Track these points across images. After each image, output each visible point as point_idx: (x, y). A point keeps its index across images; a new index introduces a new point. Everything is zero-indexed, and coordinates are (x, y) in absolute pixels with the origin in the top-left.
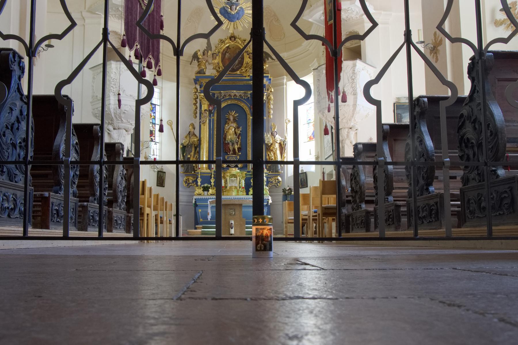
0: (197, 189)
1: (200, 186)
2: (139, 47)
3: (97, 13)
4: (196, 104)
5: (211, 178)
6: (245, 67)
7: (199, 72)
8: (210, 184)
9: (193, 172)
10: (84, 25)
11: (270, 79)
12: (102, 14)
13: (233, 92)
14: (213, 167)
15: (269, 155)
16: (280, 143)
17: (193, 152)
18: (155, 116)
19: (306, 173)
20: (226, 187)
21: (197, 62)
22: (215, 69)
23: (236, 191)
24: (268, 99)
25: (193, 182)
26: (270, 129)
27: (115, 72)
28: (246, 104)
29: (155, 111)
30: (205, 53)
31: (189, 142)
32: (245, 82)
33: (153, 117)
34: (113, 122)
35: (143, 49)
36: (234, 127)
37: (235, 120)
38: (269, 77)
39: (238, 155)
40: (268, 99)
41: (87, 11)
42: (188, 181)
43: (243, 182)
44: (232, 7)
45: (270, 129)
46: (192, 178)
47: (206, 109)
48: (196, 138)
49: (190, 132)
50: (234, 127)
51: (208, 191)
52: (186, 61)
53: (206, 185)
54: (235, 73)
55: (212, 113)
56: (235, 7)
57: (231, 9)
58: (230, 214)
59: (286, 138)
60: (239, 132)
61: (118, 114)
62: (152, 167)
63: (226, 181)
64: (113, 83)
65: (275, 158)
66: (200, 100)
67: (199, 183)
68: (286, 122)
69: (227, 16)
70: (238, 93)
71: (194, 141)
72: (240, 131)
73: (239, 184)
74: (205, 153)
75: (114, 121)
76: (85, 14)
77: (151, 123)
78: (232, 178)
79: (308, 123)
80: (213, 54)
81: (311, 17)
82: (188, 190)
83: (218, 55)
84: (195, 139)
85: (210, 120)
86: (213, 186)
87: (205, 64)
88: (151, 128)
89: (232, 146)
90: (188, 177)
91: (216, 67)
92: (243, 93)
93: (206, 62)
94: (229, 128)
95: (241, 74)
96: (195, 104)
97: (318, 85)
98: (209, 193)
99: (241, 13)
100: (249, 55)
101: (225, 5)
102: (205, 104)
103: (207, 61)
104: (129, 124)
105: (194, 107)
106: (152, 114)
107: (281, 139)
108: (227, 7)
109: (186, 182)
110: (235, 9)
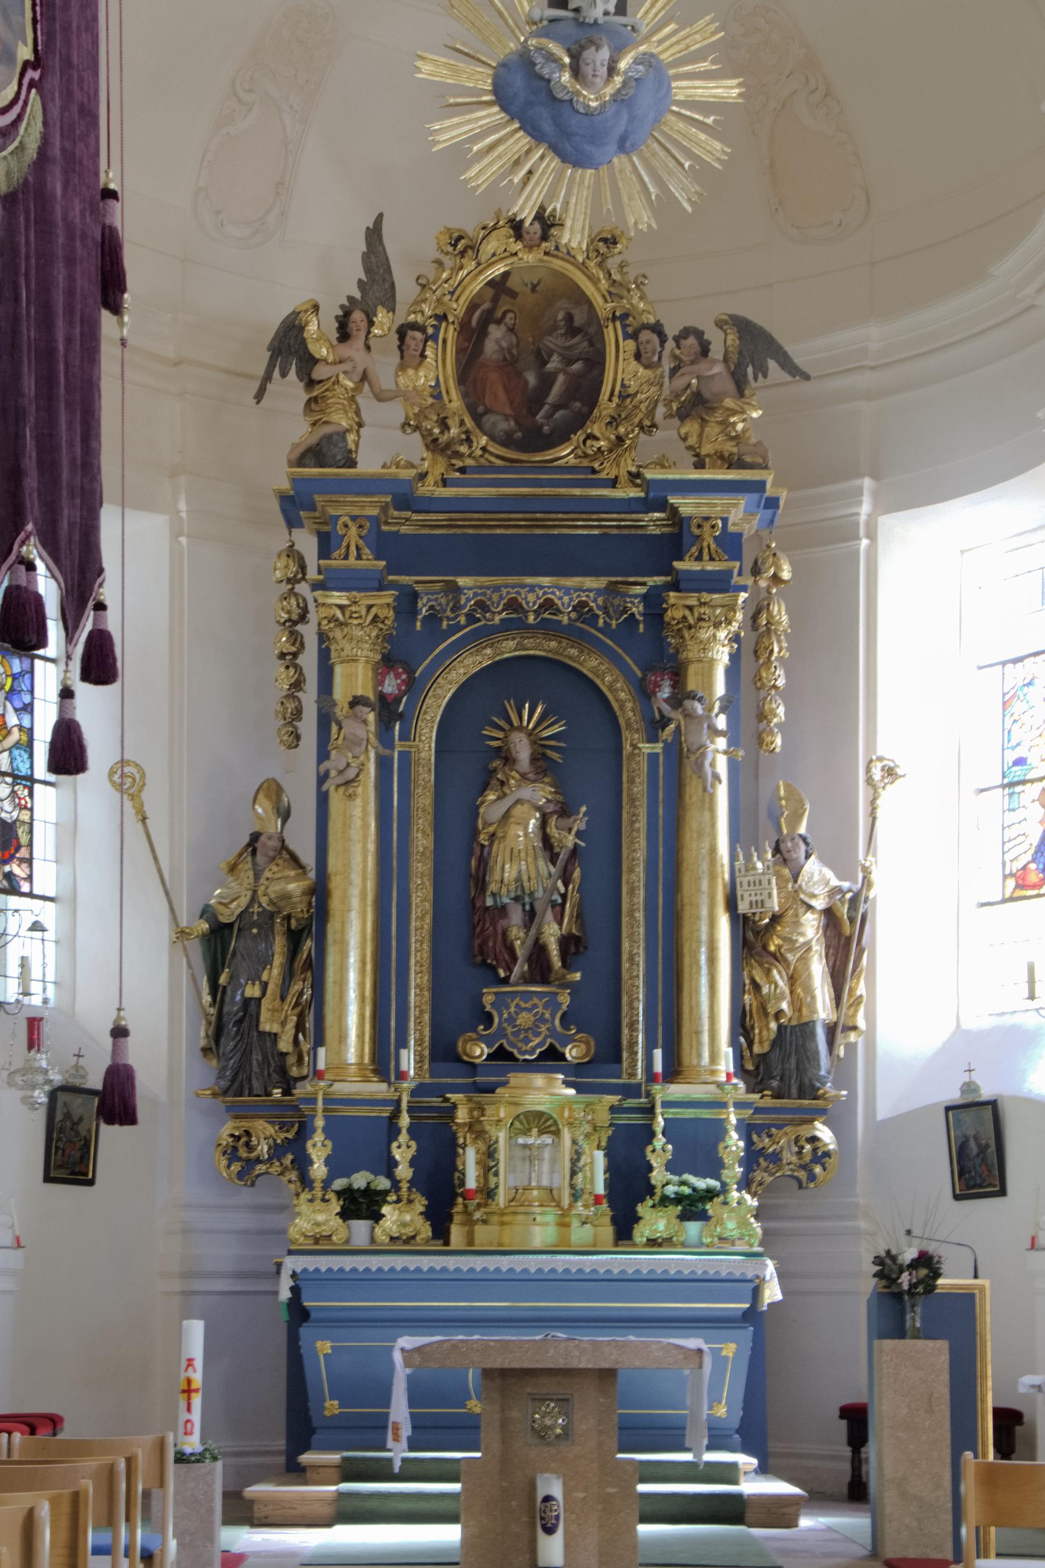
1: (327, 1184)
4: (295, 655)
5: (393, 1132)
6: (614, 421)
9: (277, 1093)
13: (532, 588)
15: (756, 987)
16: (829, 913)
18: (30, 731)
19: (993, 1104)
20: (490, 1194)
22: (417, 428)
23: (550, 1218)
25: (277, 1151)
29: (27, 699)
31: (254, 899)
32: (611, 520)
33: (15, 735)
36: (539, 809)
42: (247, 1144)
44: (589, 54)
46: (271, 1130)
47: (360, 692)
48: (296, 879)
49: (255, 837)
50: (539, 809)
51: (377, 1217)
53: (360, 1180)
54: (549, 455)
55: (401, 716)
56: (605, 54)
57: (576, 72)
58: (541, 1434)
59: (867, 883)
60: (570, 840)
62: (19, 1079)
63: (490, 1153)
65: (797, 1005)
66: (323, 637)
67: (319, 1170)
68: (869, 781)
69: (547, 126)
70: (567, 591)
71: (286, 897)
72: (579, 835)
73: (573, 1173)
74: (355, 903)
78: (526, 1132)
80: (402, 332)
82: (246, 1195)
83: (434, 337)
84: (292, 886)
85: (384, 765)
86: (404, 1186)
88: (7, 806)
90: (245, 1124)
91: (422, 415)
92: (599, 592)
93: (357, 389)
94: (507, 815)
95: (585, 463)
96: (290, 658)
98: (378, 1231)
100: (634, 336)
101: (533, 42)
102: (354, 660)
103: (364, 377)
105: (284, 678)
107: (835, 882)
108: (551, 58)
109: (232, 1154)
110: (603, 71)
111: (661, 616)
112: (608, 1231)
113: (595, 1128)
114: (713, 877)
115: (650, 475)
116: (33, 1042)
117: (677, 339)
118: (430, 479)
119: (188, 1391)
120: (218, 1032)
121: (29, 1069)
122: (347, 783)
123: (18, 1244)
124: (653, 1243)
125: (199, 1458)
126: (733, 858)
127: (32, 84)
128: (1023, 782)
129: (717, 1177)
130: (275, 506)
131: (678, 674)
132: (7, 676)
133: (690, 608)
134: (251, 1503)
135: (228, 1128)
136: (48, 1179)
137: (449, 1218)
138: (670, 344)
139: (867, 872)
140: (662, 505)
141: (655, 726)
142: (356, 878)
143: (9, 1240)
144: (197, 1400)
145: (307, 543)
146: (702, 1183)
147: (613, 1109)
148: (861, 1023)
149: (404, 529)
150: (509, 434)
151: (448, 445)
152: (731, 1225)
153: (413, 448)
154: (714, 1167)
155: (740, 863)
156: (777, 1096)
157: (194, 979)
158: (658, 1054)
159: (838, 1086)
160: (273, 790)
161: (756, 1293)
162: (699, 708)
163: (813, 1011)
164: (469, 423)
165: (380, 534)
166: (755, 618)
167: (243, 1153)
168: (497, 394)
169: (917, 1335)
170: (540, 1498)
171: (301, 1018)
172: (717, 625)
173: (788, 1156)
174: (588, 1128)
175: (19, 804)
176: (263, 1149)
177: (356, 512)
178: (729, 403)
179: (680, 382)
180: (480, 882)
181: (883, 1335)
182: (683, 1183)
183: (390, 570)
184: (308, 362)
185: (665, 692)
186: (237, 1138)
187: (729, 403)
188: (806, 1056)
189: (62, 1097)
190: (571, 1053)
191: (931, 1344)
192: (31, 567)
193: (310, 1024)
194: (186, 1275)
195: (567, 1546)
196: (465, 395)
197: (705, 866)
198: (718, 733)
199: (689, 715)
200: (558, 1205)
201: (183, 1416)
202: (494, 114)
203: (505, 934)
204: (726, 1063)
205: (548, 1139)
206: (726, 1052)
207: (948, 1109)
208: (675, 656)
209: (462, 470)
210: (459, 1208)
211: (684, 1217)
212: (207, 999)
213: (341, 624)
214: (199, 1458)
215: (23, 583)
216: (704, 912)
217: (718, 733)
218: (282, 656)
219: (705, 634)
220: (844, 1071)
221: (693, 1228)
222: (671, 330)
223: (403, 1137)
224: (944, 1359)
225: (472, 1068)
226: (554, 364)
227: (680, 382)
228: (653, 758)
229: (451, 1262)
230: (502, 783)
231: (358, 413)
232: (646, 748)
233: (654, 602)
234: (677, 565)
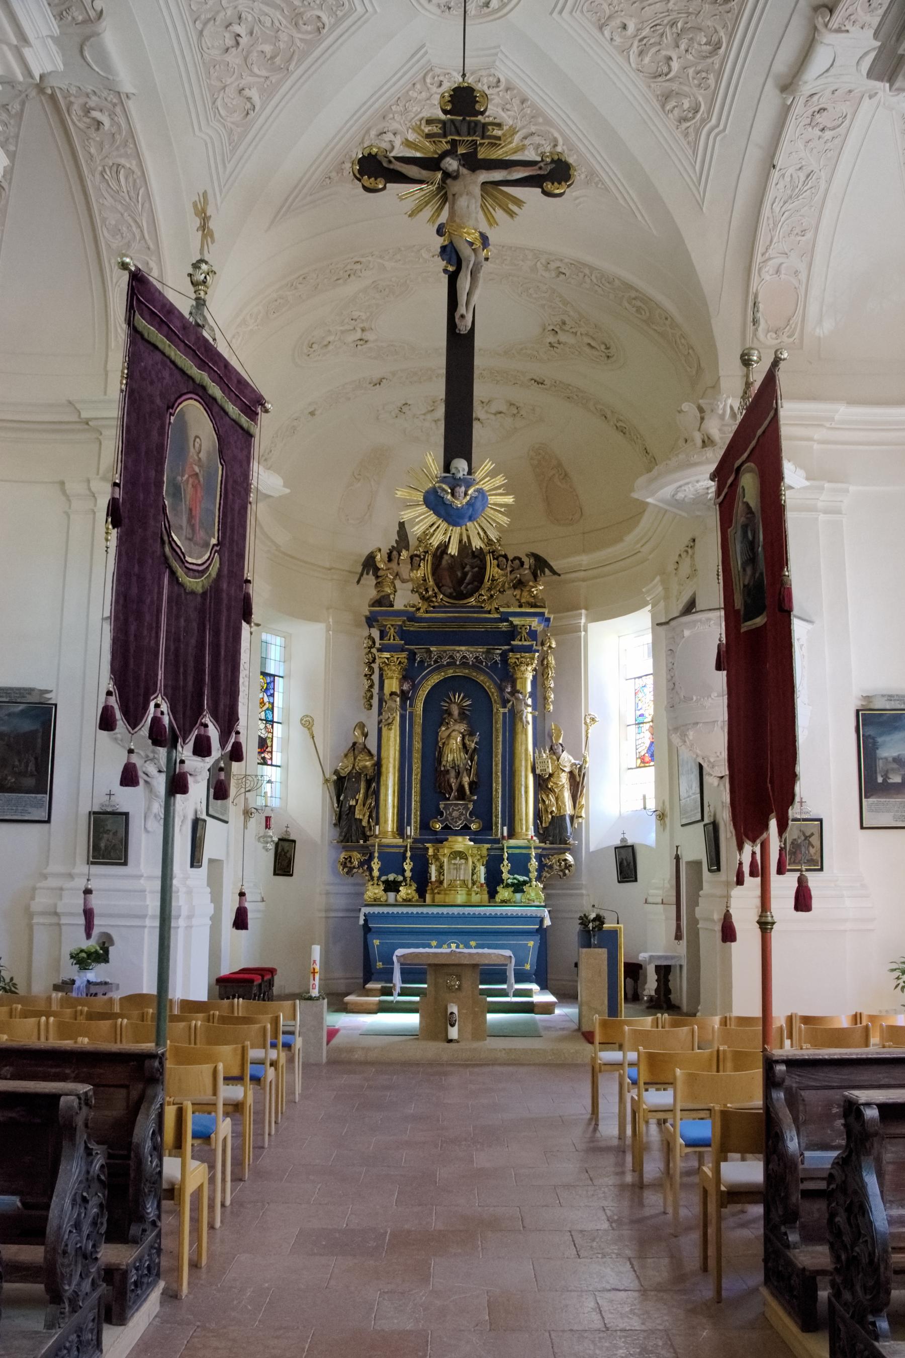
0: (370, 887)
1: (379, 878)
2: (164, 707)
4: (371, 675)
5: (405, 859)
6: (490, 589)
7: (378, 602)
8: (404, 876)
9: (361, 842)
11: (548, 620)
13: (458, 651)
14: (409, 833)
15: (544, 801)
16: (571, 773)
17: (362, 791)
18: (273, 704)
19: (632, 847)
20: (441, 882)
21: (373, 578)
22: (417, 591)
23: (464, 892)
24: (542, 664)
25: (361, 864)
26: (547, 738)
28: (491, 678)
29: (272, 691)
30: (393, 557)
31: (353, 767)
32: (489, 626)
33: (267, 705)
35: (180, 708)
36: (462, 733)
37: (463, 716)
38: (546, 615)
39: (470, 801)
40: (542, 664)
42: (350, 861)
43: (482, 870)
44: (457, 489)
45: (547, 738)
46: (359, 856)
47: (394, 690)
48: (369, 760)
49: (354, 744)
50: (462, 733)
51: (398, 891)
52: (350, 572)
53: (391, 877)
54: (465, 602)
55: (409, 698)
56: (463, 489)
57: (453, 494)
58: (450, 988)
59: (585, 761)
60: (473, 745)
62: (262, 840)
63: (441, 867)
65: (559, 809)
66: (381, 669)
67: (376, 873)
68: (586, 723)
69: (443, 512)
70: (471, 652)
71: (365, 767)
72: (476, 743)
73: (473, 875)
74: (391, 769)
77: (261, 719)
78: (455, 858)
79: (639, 724)
80: (412, 558)
81: (652, 494)
82: (351, 880)
83: (424, 559)
84: (367, 763)
85: (403, 717)
86: (408, 879)
87: (393, 583)
88: (263, 731)
89: (457, 778)
90: (349, 854)
91: (419, 586)
92: (483, 652)
93: (395, 578)
94: (449, 736)
95: (479, 604)
96: (369, 676)
97: (670, 665)
98: (398, 897)
99: (478, 504)
100: (497, 559)
101: (437, 485)
102: (392, 678)
103: (397, 574)
105: (367, 684)
106: (266, 699)
107: (573, 761)
108: (443, 490)
109: (344, 865)
110: (463, 495)
111: (507, 660)
112: (486, 897)
113: (482, 857)
114: (526, 760)
115: (502, 610)
116: (268, 826)
117: (512, 561)
118: (422, 611)
119: (314, 973)
120: (340, 818)
121: (265, 836)
122: (389, 724)
124: (503, 901)
125: (317, 999)
126: (534, 753)
127: (216, 551)
128: (643, 723)
129: (528, 876)
130: (364, 619)
131: (514, 683)
133: (518, 659)
134: (347, 1004)
135: (343, 855)
136: (275, 874)
137: (426, 891)
138: (510, 562)
139: (585, 758)
140: (507, 621)
141: (505, 703)
142: (391, 760)
143: (259, 899)
144: (317, 976)
145: (376, 634)
146: (521, 878)
147: (488, 849)
148: (583, 815)
149: (412, 629)
150: (451, 594)
151: (429, 598)
152: (533, 894)
153: (416, 599)
154: (526, 872)
155: (537, 755)
156: (551, 843)
157: (331, 798)
158: (505, 828)
159: (574, 839)
160: (361, 726)
161: (542, 920)
162: (521, 696)
163: (565, 811)
164: (436, 590)
165: (403, 630)
166: (542, 661)
167: (348, 865)
168: (447, 581)
169: (596, 946)
170: (449, 1012)
171: (371, 812)
172: (527, 665)
173: (556, 867)
174: (479, 857)
176: (356, 863)
177: (393, 623)
178: (531, 583)
179: (513, 576)
180: (440, 762)
181: (584, 946)
182: (515, 879)
183: (406, 644)
184: (376, 569)
185: (509, 690)
186: (346, 859)
187: (531, 583)
188: (563, 828)
189: (281, 843)
190: (473, 827)
191: (600, 950)
192: (206, 726)
193: (374, 815)
194: (327, 911)
195: (459, 1030)
196: (435, 580)
197: (523, 756)
198: (529, 706)
199: (517, 699)
200: (467, 887)
201: (312, 982)
202: (424, 508)
203: (448, 780)
204: (531, 832)
205: (463, 861)
206: (531, 827)
207: (616, 848)
208: (512, 676)
209: (434, 607)
210: (429, 888)
211: (514, 892)
212: (336, 805)
213: (387, 665)
214: (317, 999)
215: (202, 733)
216: (523, 774)
217: (529, 706)
218: (366, 675)
219: (523, 668)
220: (577, 833)
221: (518, 896)
222: (510, 557)
223: (408, 861)
224: (606, 956)
225: (435, 832)
226: (467, 568)
227: (513, 576)
228: (504, 714)
229: (425, 910)
230: (447, 724)
231: (395, 587)
232: (502, 710)
233: (504, 655)
234: (513, 642)
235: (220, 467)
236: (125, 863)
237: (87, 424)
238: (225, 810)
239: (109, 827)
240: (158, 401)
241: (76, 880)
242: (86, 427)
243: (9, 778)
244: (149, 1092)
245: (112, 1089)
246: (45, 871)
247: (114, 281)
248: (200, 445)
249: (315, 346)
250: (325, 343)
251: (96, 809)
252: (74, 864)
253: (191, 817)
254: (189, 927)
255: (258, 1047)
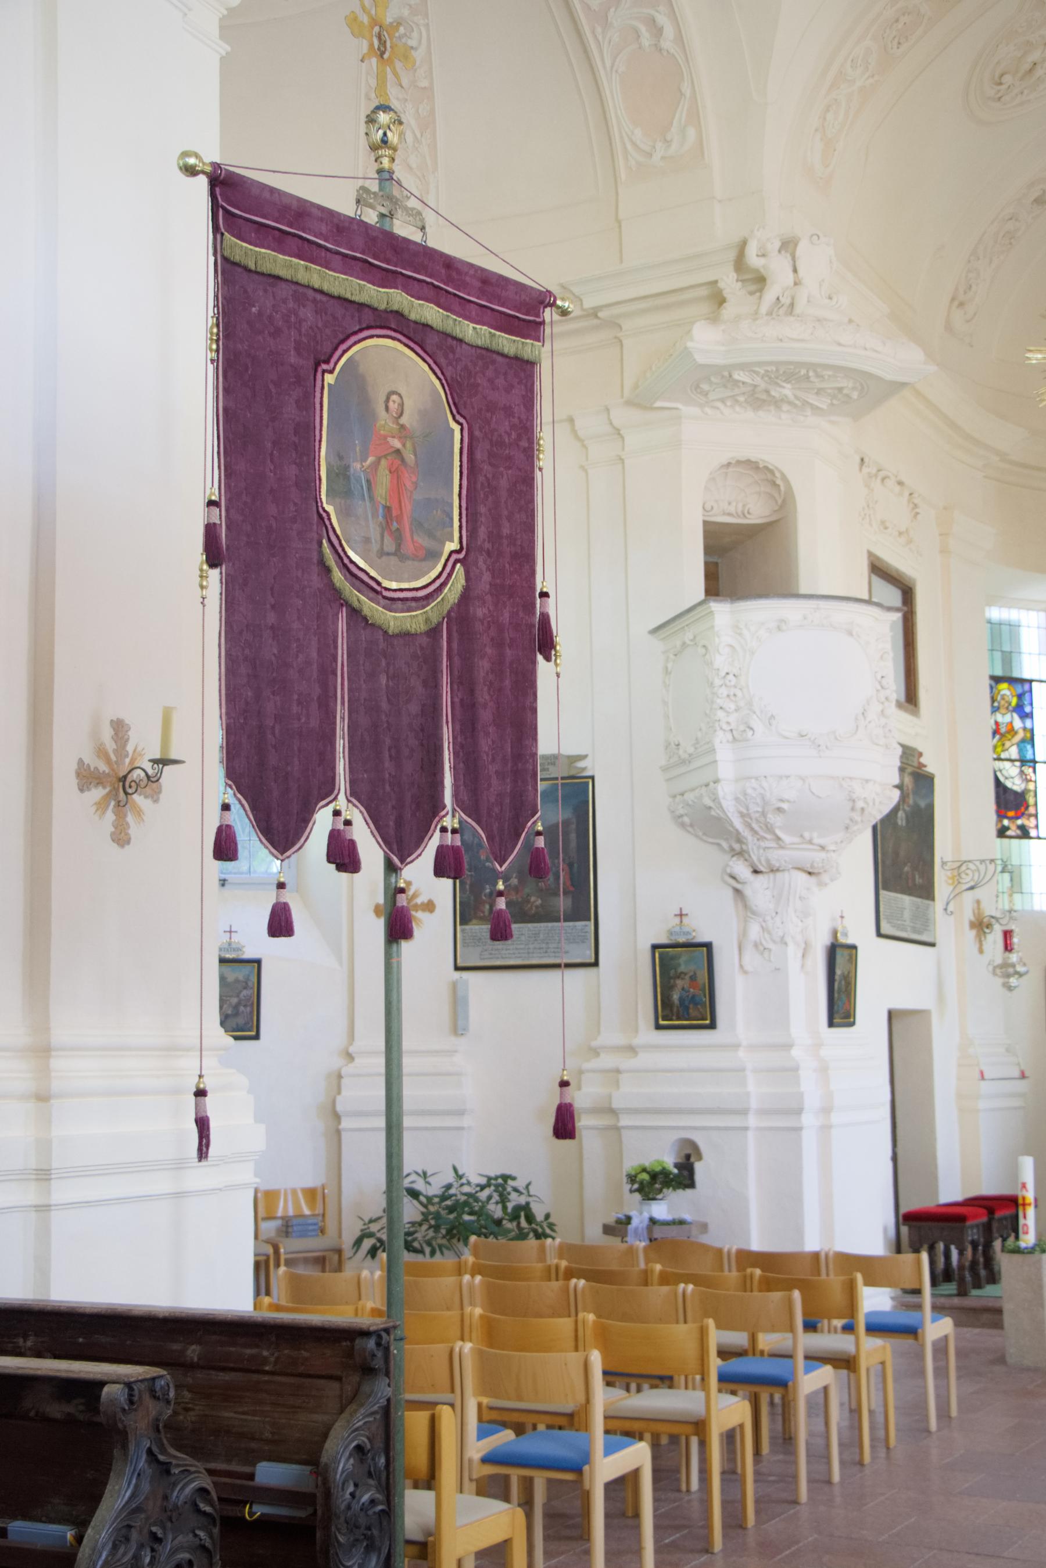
3: (658, 404)
10: (622, 460)
12: (679, 406)
18: (1032, 731)
27: (731, 646)
33: (1021, 735)
34: (744, 847)
41: (629, 403)
61: (754, 816)
62: (998, 971)
64: (724, 691)
75: (746, 844)
76: (621, 416)
88: (1018, 781)
104: (811, 847)
121: (1005, 965)
123: (1023, 1076)
132: (1013, 696)
143: (1017, 1073)
175: (1026, 779)
235: (457, 428)
236: (712, 1026)
237: (596, 317)
238: (924, 921)
239: (682, 968)
240: (293, 359)
241: (602, 1055)
242: (596, 321)
243: (533, 899)
244: (366, 1388)
245: (322, 1382)
246: (594, 1044)
247: (608, 64)
248: (402, 405)
249: (1007, 79)
250: (1027, 66)
251: (663, 940)
252: (636, 1030)
253: (821, 942)
254: (826, 1129)
255: (786, 1331)
